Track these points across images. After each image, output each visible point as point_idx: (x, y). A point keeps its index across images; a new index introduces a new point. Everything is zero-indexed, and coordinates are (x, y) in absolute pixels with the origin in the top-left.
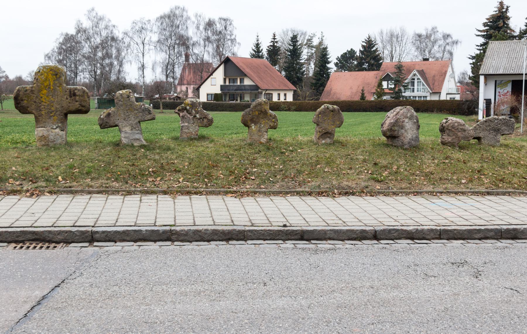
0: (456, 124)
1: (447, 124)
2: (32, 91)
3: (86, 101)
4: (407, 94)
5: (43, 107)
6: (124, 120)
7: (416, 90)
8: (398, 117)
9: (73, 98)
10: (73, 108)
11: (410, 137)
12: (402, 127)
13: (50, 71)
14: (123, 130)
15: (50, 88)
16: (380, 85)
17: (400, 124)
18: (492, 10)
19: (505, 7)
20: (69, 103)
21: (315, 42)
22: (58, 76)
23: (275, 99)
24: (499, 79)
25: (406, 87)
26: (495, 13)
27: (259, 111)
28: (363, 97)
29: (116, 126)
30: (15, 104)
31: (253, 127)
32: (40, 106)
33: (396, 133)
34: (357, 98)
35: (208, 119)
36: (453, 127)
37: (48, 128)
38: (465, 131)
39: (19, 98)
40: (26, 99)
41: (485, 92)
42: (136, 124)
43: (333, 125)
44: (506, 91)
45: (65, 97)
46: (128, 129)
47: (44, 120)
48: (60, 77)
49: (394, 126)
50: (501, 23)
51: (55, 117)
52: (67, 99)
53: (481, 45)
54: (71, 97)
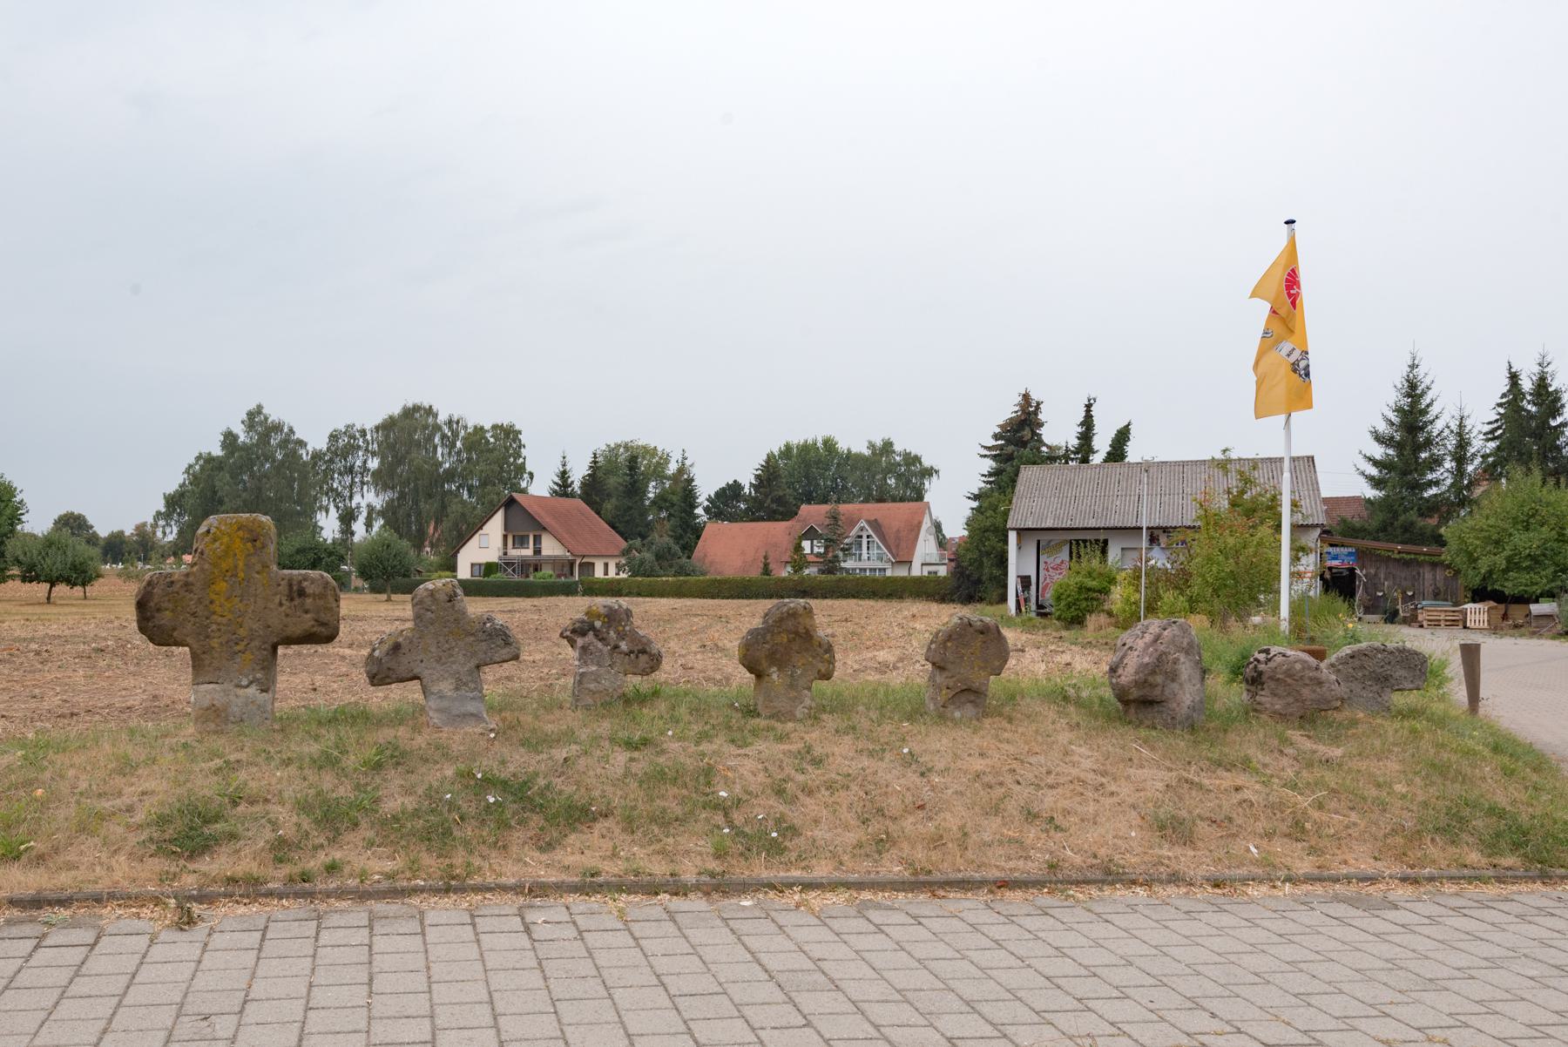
0: (1298, 666)
1: (1271, 664)
2: (186, 584)
3: (331, 609)
5: (214, 627)
6: (439, 660)
7: (865, 556)
8: (1162, 648)
10: (296, 630)
11: (1188, 703)
12: (1173, 676)
14: (435, 689)
15: (236, 576)
16: (798, 548)
17: (1168, 667)
18: (1007, 410)
21: (672, 468)
22: (258, 544)
23: (599, 573)
24: (1044, 537)
25: (847, 551)
27: (789, 632)
28: (766, 571)
29: (416, 678)
30: (139, 622)
31: (775, 676)
32: (207, 627)
33: (1157, 692)
34: (755, 573)
35: (651, 655)
36: (1289, 673)
38: (1320, 683)
41: (1019, 562)
42: (470, 672)
43: (984, 668)
44: (1058, 561)
46: (446, 687)
47: (216, 664)
48: (264, 546)
49: (1153, 673)
50: (1026, 433)
51: (248, 655)
53: (990, 475)
54: (292, 599)
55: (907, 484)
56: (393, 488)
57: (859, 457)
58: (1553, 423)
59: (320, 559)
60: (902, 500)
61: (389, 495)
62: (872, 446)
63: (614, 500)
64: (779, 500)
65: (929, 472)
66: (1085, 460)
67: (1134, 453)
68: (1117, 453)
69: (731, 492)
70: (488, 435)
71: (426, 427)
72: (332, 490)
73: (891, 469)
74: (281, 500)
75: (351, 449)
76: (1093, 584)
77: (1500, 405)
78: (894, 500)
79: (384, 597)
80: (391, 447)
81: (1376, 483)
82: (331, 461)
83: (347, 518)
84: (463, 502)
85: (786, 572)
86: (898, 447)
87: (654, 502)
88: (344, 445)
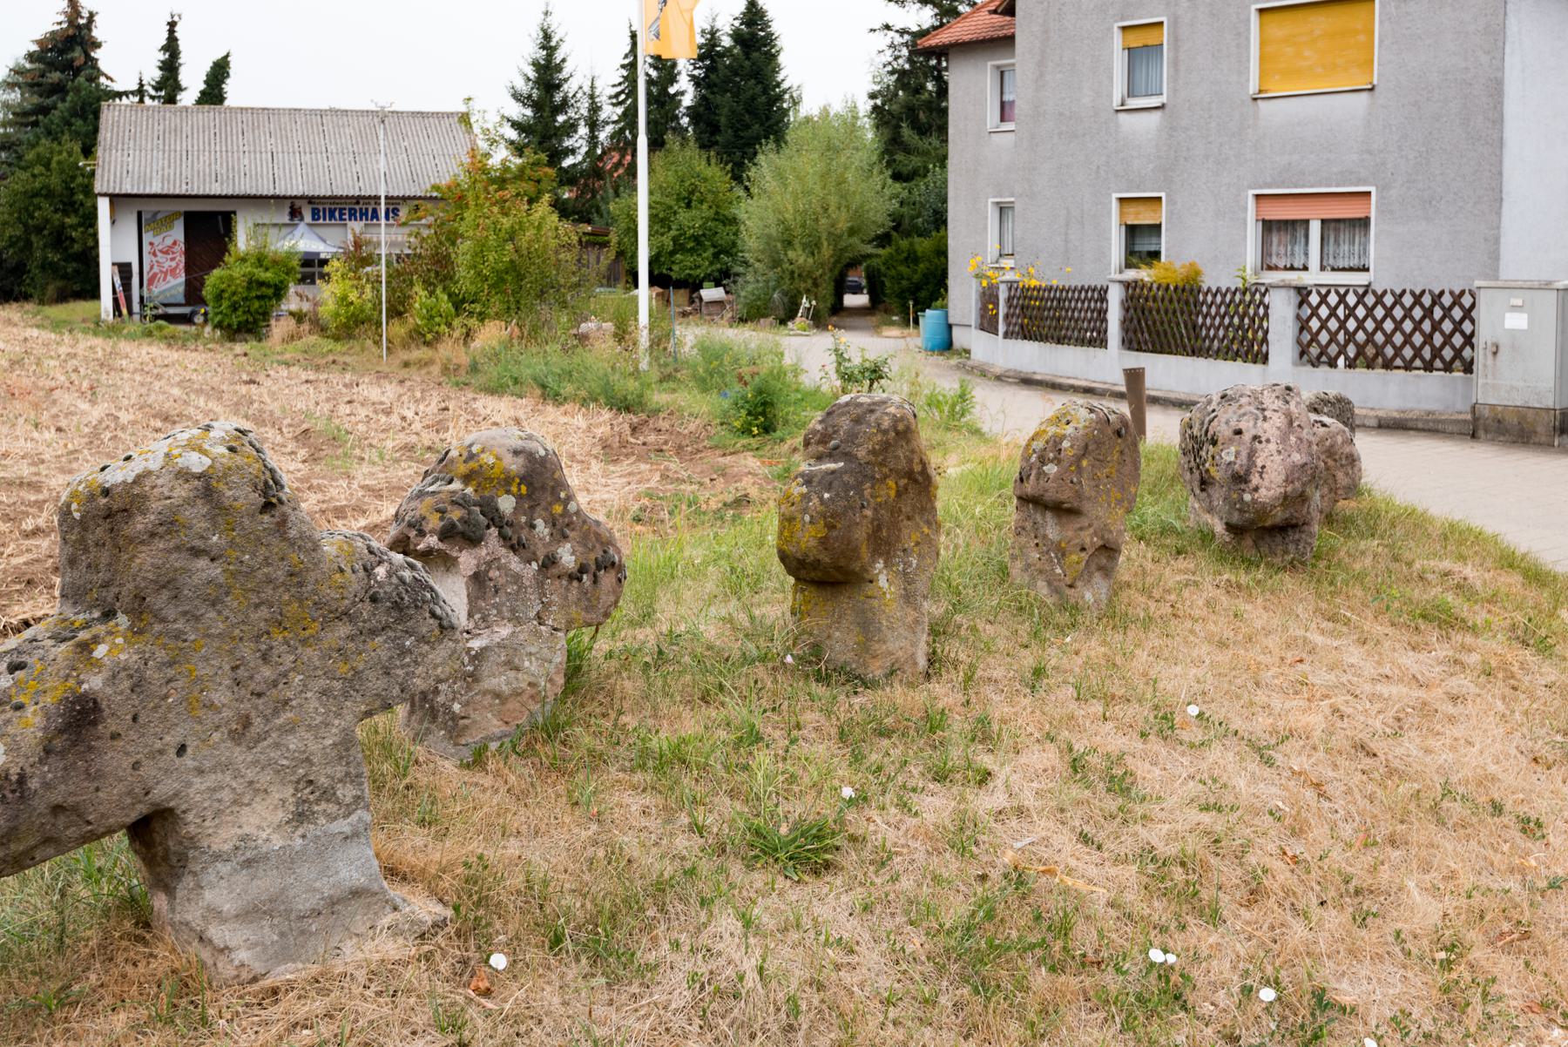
6: (241, 731)
18: (48, 17)
19: (85, 14)
24: (149, 208)
26: (57, 27)
31: (882, 581)
44: (169, 242)
50: (77, 54)
58: (672, 90)
66: (171, 100)
67: (236, 94)
68: (213, 93)
77: (623, 66)
81: (519, 150)
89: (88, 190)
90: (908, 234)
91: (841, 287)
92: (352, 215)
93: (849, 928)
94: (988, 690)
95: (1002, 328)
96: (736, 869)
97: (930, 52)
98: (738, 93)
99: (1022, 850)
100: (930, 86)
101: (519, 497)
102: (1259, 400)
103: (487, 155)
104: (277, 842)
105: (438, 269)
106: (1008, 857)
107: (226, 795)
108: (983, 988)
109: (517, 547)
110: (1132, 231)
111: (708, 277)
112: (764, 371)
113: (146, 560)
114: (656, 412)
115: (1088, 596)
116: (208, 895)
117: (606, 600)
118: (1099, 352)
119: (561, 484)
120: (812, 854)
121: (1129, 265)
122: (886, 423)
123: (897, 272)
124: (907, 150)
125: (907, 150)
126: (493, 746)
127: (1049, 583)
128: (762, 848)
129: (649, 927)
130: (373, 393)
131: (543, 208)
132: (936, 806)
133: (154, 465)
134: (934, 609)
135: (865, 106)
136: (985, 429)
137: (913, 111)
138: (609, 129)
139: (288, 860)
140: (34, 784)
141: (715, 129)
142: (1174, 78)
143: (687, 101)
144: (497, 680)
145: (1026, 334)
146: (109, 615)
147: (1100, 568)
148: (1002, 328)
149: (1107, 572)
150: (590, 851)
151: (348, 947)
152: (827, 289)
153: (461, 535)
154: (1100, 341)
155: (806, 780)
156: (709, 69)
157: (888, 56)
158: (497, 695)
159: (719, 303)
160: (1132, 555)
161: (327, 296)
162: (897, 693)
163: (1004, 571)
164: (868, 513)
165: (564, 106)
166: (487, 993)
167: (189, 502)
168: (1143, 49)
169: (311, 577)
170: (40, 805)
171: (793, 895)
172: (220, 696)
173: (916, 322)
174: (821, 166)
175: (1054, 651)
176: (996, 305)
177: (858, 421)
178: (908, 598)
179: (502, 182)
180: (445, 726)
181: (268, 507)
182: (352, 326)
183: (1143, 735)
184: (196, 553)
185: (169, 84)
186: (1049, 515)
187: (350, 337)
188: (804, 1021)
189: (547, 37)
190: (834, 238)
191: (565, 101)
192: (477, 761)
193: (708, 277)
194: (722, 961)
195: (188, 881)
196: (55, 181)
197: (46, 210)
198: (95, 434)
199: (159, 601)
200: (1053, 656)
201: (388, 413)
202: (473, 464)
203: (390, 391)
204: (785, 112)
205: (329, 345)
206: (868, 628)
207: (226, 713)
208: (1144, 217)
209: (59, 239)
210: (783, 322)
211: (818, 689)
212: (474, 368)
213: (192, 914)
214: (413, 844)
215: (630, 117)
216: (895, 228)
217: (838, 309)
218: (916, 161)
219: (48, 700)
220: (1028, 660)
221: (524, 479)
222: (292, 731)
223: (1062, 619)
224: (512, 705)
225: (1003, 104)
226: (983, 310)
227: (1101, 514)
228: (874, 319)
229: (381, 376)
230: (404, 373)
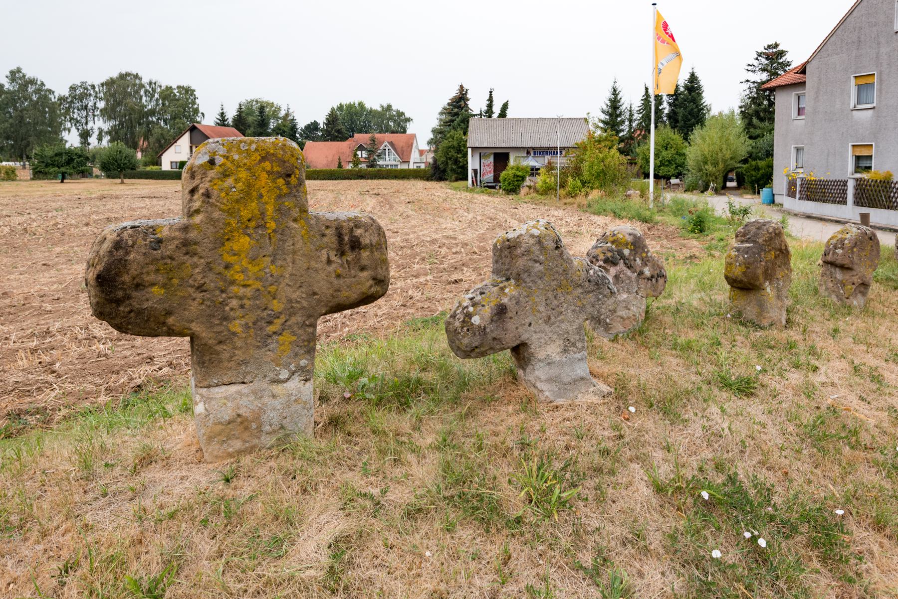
2: (186, 243)
4: (381, 162)
5: (234, 303)
6: (548, 321)
7: (387, 159)
9: (350, 256)
13: (263, 159)
15: (264, 226)
16: (355, 155)
18: (454, 92)
20: (338, 276)
21: (282, 113)
24: (483, 151)
28: (340, 166)
31: (768, 290)
32: (223, 304)
34: (334, 167)
37: (257, 384)
39: (126, 278)
40: (160, 278)
45: (324, 258)
50: (462, 103)
51: (287, 337)
52: (329, 262)
54: (342, 254)
55: (399, 125)
56: (115, 119)
57: (376, 112)
59: (73, 160)
60: (397, 132)
61: (112, 123)
62: (382, 107)
63: (252, 129)
64: (339, 131)
65: (408, 120)
66: (490, 117)
67: (510, 114)
68: (503, 114)
69: (313, 127)
70: (175, 91)
71: (135, 85)
72: (73, 119)
73: (391, 118)
74: (36, 124)
75: (84, 96)
76: (520, 174)
78: (393, 132)
79: (119, 181)
80: (113, 95)
82: (72, 102)
83: (85, 135)
84: (161, 127)
85: (350, 166)
86: (394, 108)
87: (273, 130)
88: (79, 95)
89: (465, 146)
90: (755, 160)
91: (726, 179)
92: (547, 153)
93: (763, 418)
94: (813, 335)
95: (798, 196)
96: (716, 391)
97: (765, 90)
98: (687, 107)
99: (834, 399)
100: (765, 103)
101: (631, 250)
102: (45, 426)
103: (594, 132)
104: (558, 358)
105: (577, 171)
106: (829, 401)
107: (542, 340)
108: (821, 449)
109: (629, 267)
110: (858, 158)
111: (673, 175)
112: (700, 210)
113: (521, 263)
114: (657, 223)
115: (855, 303)
116: (537, 372)
117: (660, 288)
118: (843, 206)
119: (645, 246)
120: (745, 388)
121: (856, 172)
122: (771, 230)
123: (753, 174)
124: (755, 127)
125: (755, 127)
126: (621, 335)
127: (837, 296)
128: (725, 384)
129: (684, 406)
130: (556, 213)
131: (614, 151)
132: (796, 378)
133: (523, 232)
134: (788, 302)
135: (737, 111)
136: (793, 234)
137: (759, 112)
138: (637, 122)
139: (561, 365)
140: (488, 330)
141: (677, 121)
142: (879, 96)
143: (666, 111)
144: (623, 313)
145: (809, 198)
146: (508, 279)
147: (860, 292)
148: (798, 196)
149: (864, 294)
150: (659, 376)
151: (580, 396)
152: (720, 180)
153: (610, 262)
154: (844, 202)
155: (740, 361)
156: (675, 100)
157: (748, 92)
158: (622, 318)
159: (678, 185)
160: (875, 288)
161: (539, 180)
162: (775, 333)
163: (816, 291)
164: (763, 263)
165: (620, 114)
166: (628, 419)
167: (534, 245)
168: (864, 86)
169: (570, 272)
170: (490, 337)
171: (739, 403)
172: (542, 309)
173: (759, 193)
174: (719, 134)
175: (841, 323)
176: (796, 187)
177: (758, 229)
178: (779, 297)
179: (599, 141)
180: (603, 326)
181: (557, 248)
182: (547, 191)
183: (886, 361)
184: (536, 261)
185: (489, 112)
186: (837, 269)
187: (546, 194)
188: (748, 450)
189: (615, 90)
190: (724, 161)
191: (621, 113)
192: (615, 340)
193: (673, 175)
194: (714, 423)
195: (530, 367)
196: (455, 143)
197: (453, 153)
198: (470, 223)
199: (524, 276)
200: (841, 325)
201: (561, 220)
202: (615, 238)
203: (561, 213)
204: (705, 114)
205: (539, 197)
206: (761, 307)
207: (544, 314)
208: (864, 152)
209: (456, 162)
210: (702, 192)
211: (741, 328)
212: (589, 206)
213: (531, 378)
214: (597, 365)
215: (646, 118)
216: (750, 157)
217: (724, 187)
218: (758, 132)
219: (492, 304)
220: (831, 325)
221: (632, 244)
222: (563, 322)
223: (845, 311)
224: (627, 322)
225: (799, 109)
226: (789, 189)
227: (862, 270)
228: (740, 192)
229: (557, 208)
230: (565, 207)
